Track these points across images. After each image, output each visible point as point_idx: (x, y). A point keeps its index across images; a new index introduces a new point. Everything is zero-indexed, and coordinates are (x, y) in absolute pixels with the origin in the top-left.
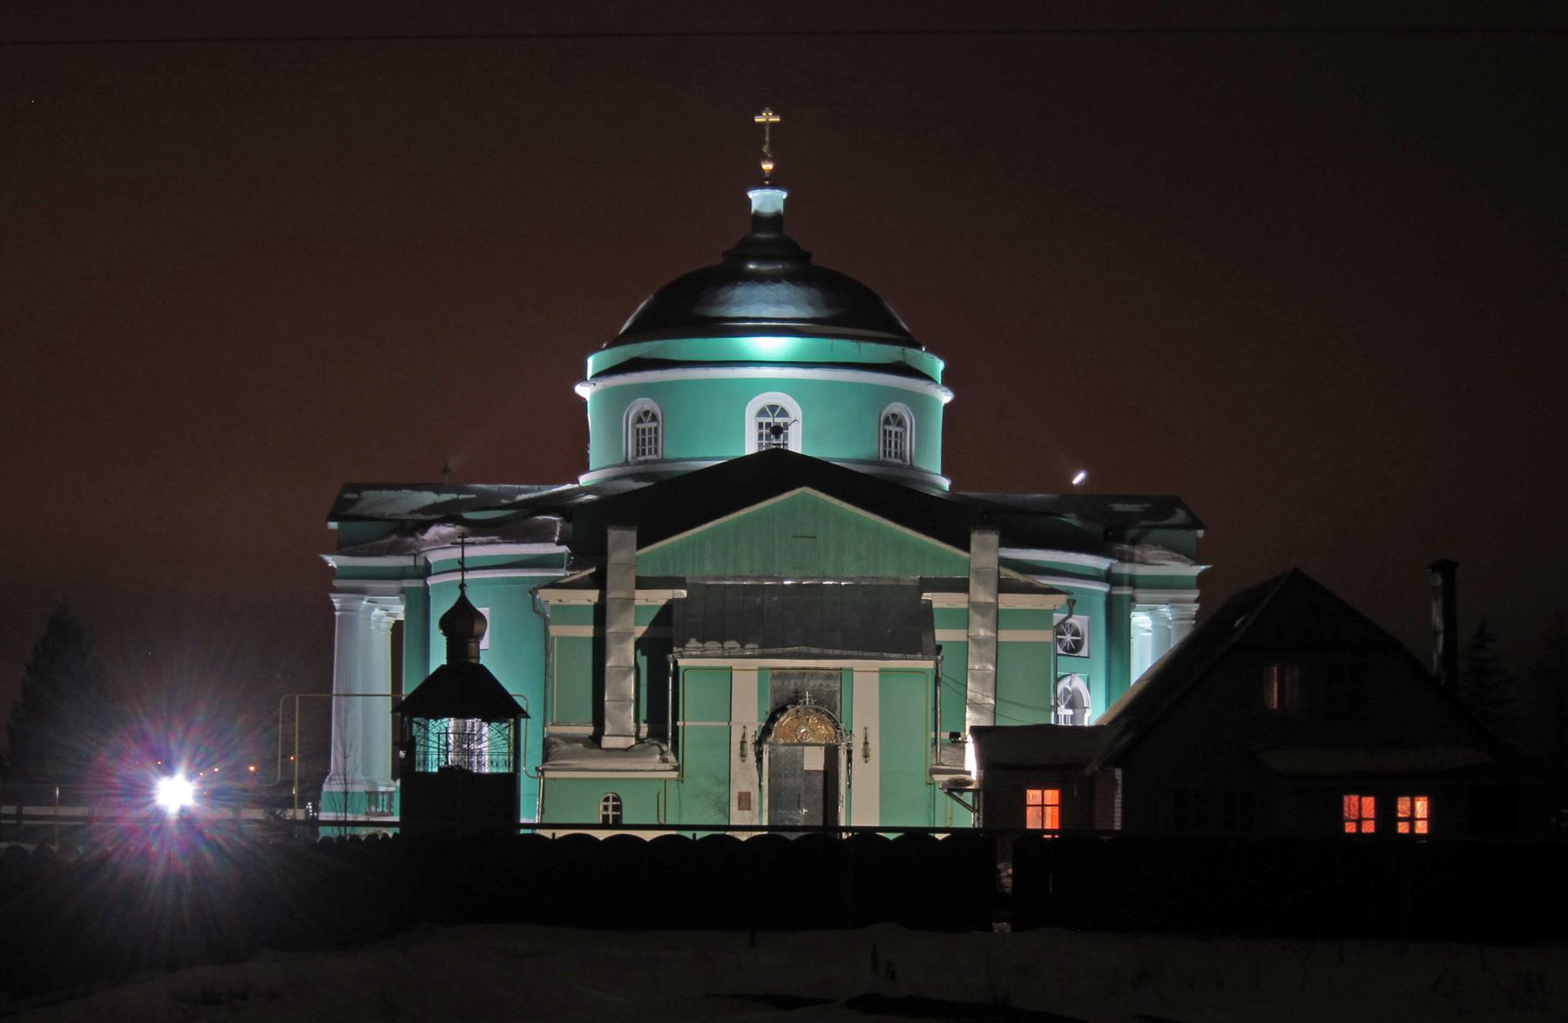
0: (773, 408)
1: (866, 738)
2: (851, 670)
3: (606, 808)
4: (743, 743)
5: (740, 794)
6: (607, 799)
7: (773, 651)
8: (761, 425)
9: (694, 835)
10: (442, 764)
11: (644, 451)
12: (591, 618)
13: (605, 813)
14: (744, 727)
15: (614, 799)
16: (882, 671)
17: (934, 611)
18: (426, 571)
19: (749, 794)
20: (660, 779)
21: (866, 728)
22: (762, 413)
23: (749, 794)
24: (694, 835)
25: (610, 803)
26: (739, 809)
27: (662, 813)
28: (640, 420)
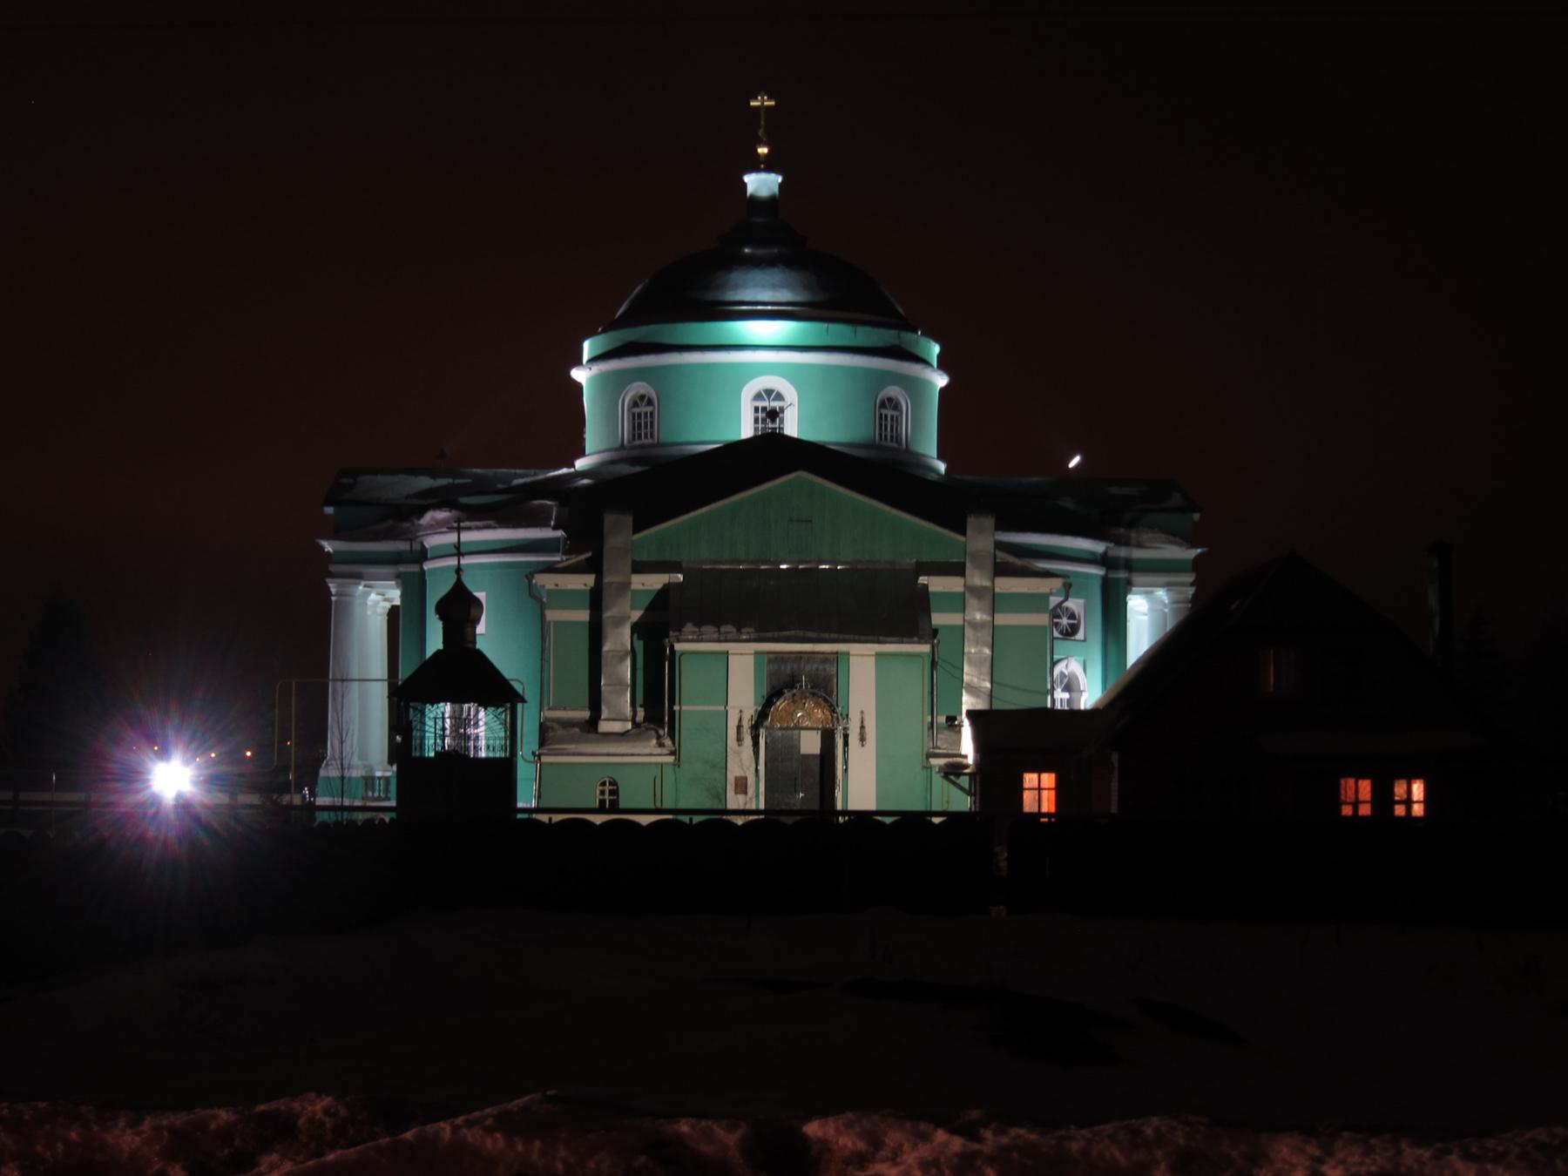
2: (848, 654)
7: (769, 635)
14: (741, 711)
16: (879, 655)
17: (931, 596)
18: (422, 556)
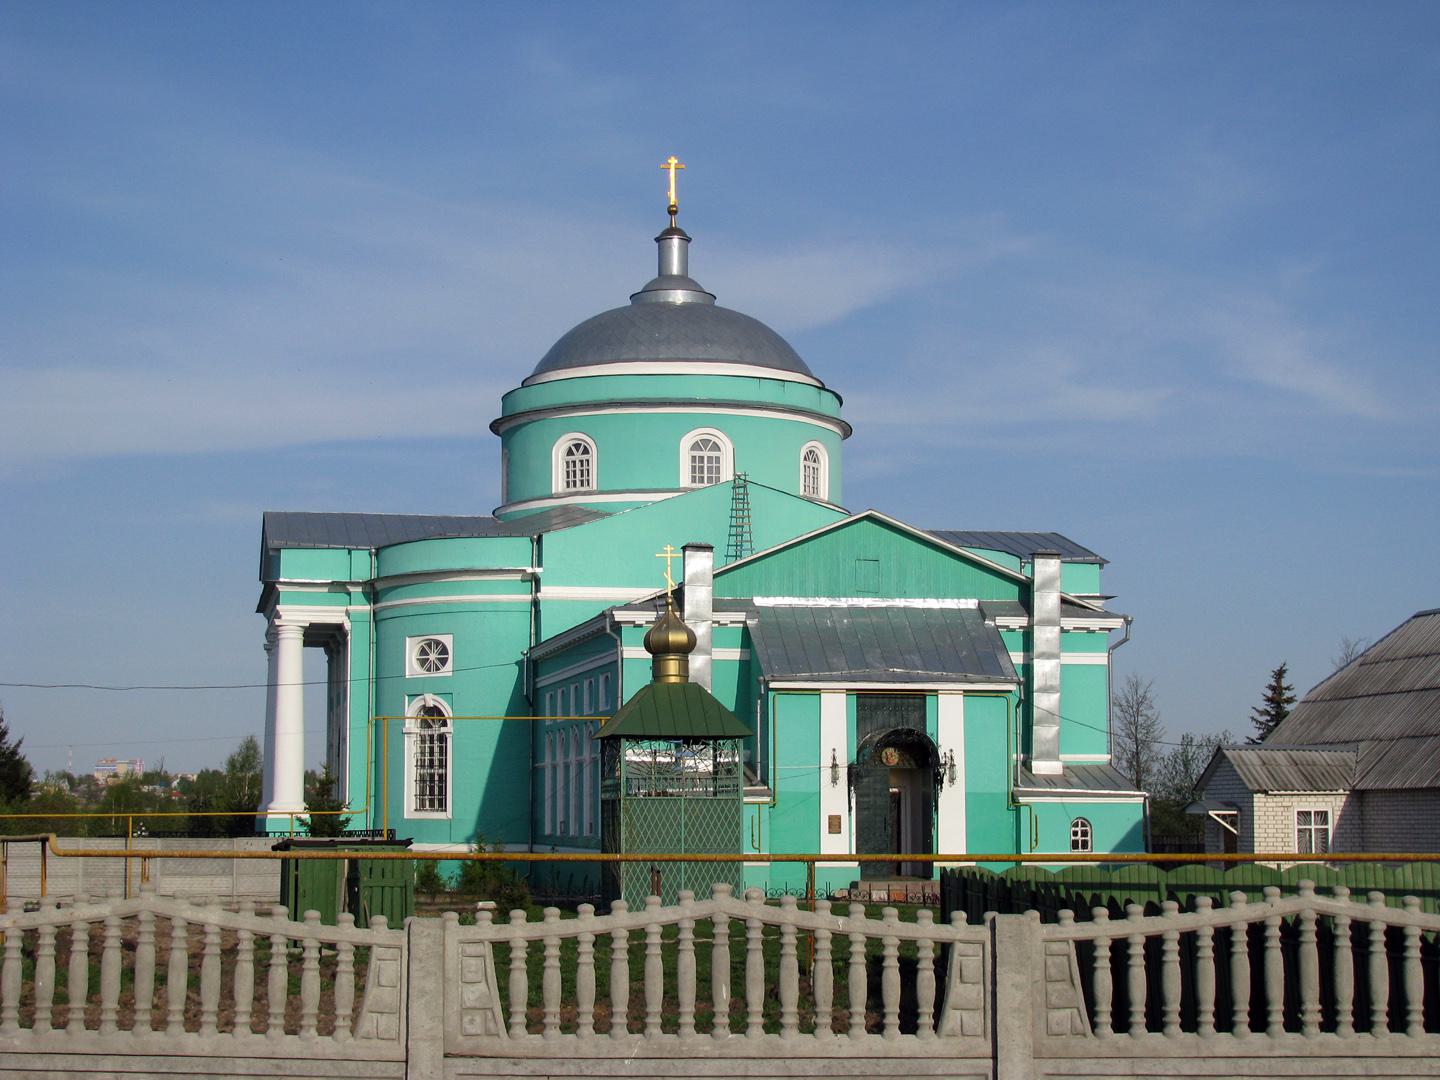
0: (706, 442)
1: (834, 759)
3: (1075, 834)
4: (834, 766)
5: (830, 817)
6: (1076, 825)
8: (694, 458)
9: (1279, 866)
10: (1349, 788)
11: (575, 482)
12: (739, 640)
13: (1073, 838)
14: (834, 750)
15: (1076, 825)
19: (839, 818)
20: (754, 803)
21: (834, 750)
22: (696, 446)
23: (839, 818)
24: (1279, 866)
25: (1079, 829)
26: (830, 833)
27: (756, 838)
28: (570, 452)
